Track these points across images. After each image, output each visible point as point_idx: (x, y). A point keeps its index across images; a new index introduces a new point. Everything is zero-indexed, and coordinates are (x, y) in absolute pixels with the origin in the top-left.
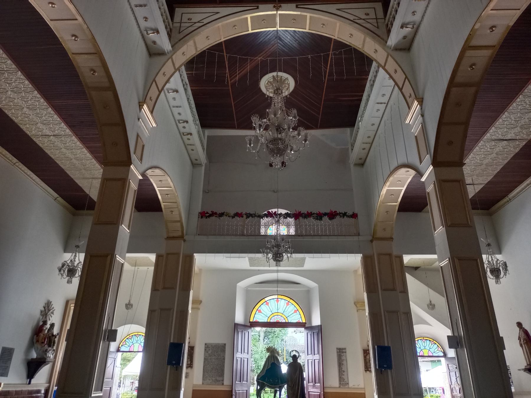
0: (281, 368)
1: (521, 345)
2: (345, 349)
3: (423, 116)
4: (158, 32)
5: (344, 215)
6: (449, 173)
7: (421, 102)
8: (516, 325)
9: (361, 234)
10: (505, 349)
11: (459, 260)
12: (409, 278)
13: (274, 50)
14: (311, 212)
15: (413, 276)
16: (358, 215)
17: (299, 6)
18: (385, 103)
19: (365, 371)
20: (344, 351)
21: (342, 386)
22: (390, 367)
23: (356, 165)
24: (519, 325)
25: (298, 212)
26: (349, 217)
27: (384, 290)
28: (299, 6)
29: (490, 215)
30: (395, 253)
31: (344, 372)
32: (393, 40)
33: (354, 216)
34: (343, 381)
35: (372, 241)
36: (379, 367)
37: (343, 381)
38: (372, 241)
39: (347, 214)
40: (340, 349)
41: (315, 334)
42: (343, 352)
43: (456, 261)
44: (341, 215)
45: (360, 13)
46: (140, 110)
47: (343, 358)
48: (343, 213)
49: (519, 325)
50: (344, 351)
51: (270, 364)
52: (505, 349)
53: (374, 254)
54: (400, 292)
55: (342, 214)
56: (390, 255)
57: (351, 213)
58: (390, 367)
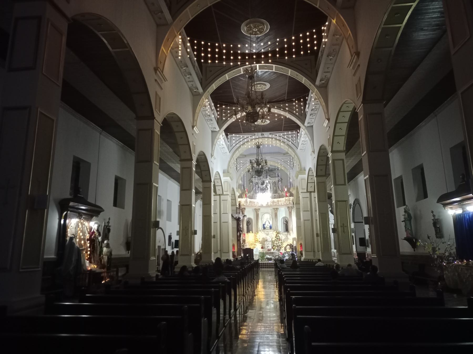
4: (212, 120)
7: (329, 119)
32: (318, 82)
46: (193, 128)
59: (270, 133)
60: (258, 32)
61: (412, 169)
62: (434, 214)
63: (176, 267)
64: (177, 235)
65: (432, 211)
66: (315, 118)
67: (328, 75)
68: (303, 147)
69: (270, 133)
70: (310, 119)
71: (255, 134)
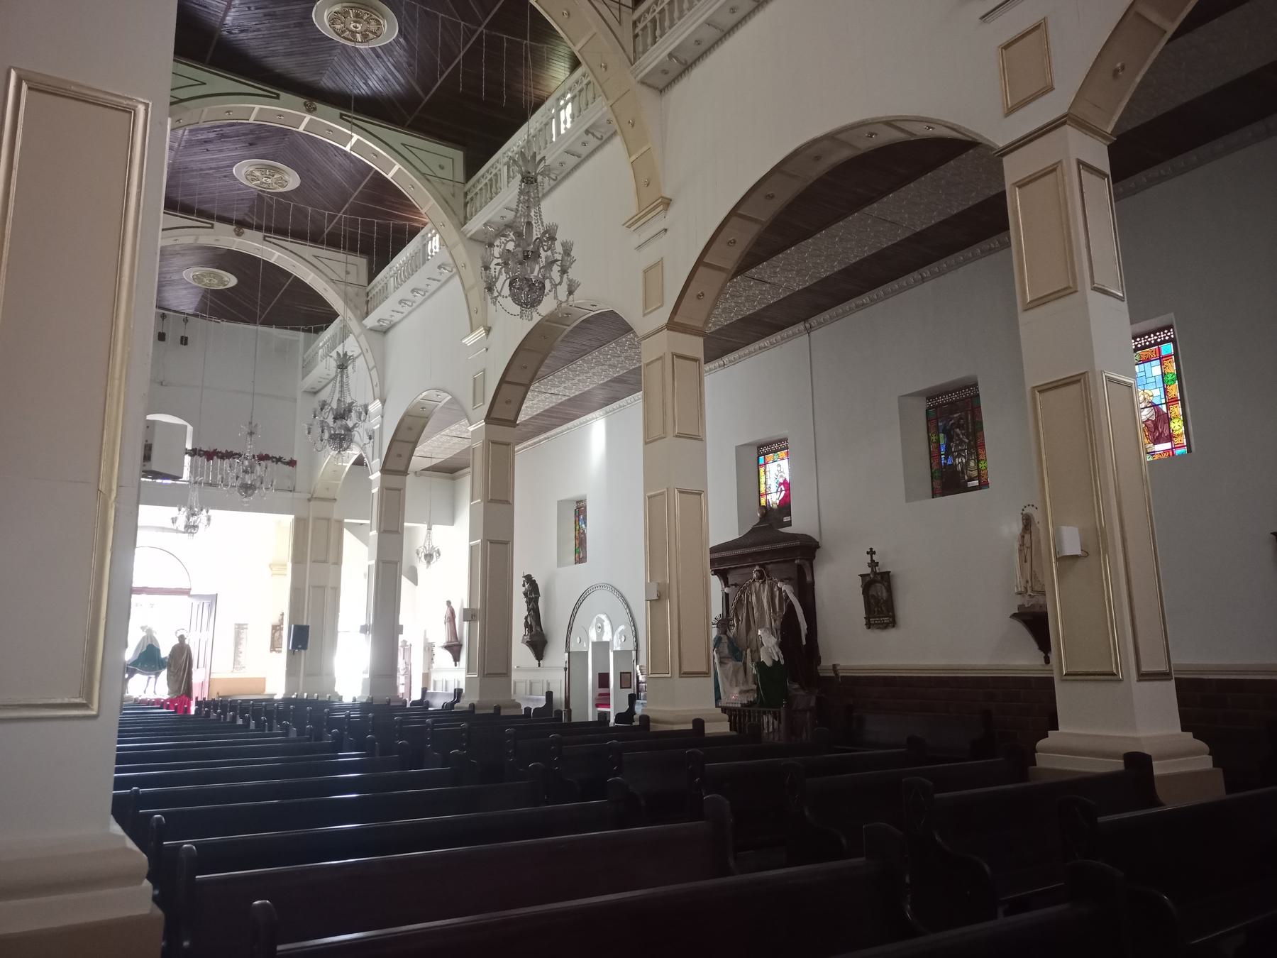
0: (1037, 647)
1: (445, 623)
2: (246, 624)
3: (382, 417)
5: (279, 460)
6: (394, 480)
8: (446, 603)
9: (297, 489)
10: (402, 634)
11: (383, 563)
12: (347, 535)
13: (200, 165)
14: (231, 452)
15: (354, 535)
16: (298, 463)
17: (267, 238)
18: (579, 157)
19: (271, 651)
20: (245, 627)
21: (235, 671)
22: (305, 647)
23: (306, 392)
24: (449, 603)
25: (212, 450)
26: (284, 463)
27: (314, 562)
28: (267, 238)
29: (454, 479)
30: (335, 516)
31: (241, 653)
32: (371, 321)
33: (292, 463)
34: (239, 664)
35: (309, 500)
36: (293, 647)
37: (239, 664)
38: (309, 500)
39: (282, 460)
40: (239, 625)
41: (205, 605)
42: (243, 629)
43: (381, 564)
44: (274, 460)
45: (340, 269)
47: (243, 636)
48: (278, 457)
49: (449, 603)
50: (245, 627)
51: (145, 647)
52: (402, 634)
53: (309, 517)
54: (333, 564)
55: (275, 458)
56: (328, 520)
57: (288, 459)
58: (305, 647)
59: (265, 236)
60: (358, 36)
61: (899, 397)
62: (874, 559)
63: (1041, 744)
64: (1047, 737)
65: (871, 549)
66: (583, 157)
67: (572, 161)
68: (321, 380)
69: (265, 236)
70: (393, 311)
71: (212, 224)
